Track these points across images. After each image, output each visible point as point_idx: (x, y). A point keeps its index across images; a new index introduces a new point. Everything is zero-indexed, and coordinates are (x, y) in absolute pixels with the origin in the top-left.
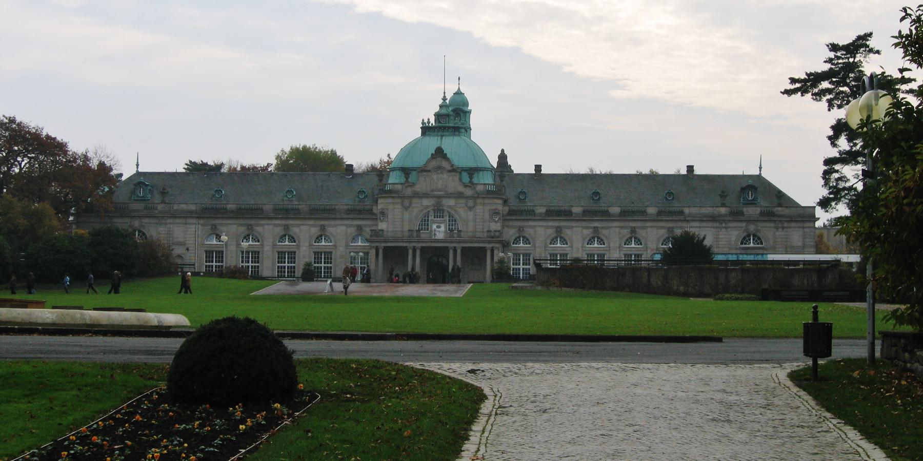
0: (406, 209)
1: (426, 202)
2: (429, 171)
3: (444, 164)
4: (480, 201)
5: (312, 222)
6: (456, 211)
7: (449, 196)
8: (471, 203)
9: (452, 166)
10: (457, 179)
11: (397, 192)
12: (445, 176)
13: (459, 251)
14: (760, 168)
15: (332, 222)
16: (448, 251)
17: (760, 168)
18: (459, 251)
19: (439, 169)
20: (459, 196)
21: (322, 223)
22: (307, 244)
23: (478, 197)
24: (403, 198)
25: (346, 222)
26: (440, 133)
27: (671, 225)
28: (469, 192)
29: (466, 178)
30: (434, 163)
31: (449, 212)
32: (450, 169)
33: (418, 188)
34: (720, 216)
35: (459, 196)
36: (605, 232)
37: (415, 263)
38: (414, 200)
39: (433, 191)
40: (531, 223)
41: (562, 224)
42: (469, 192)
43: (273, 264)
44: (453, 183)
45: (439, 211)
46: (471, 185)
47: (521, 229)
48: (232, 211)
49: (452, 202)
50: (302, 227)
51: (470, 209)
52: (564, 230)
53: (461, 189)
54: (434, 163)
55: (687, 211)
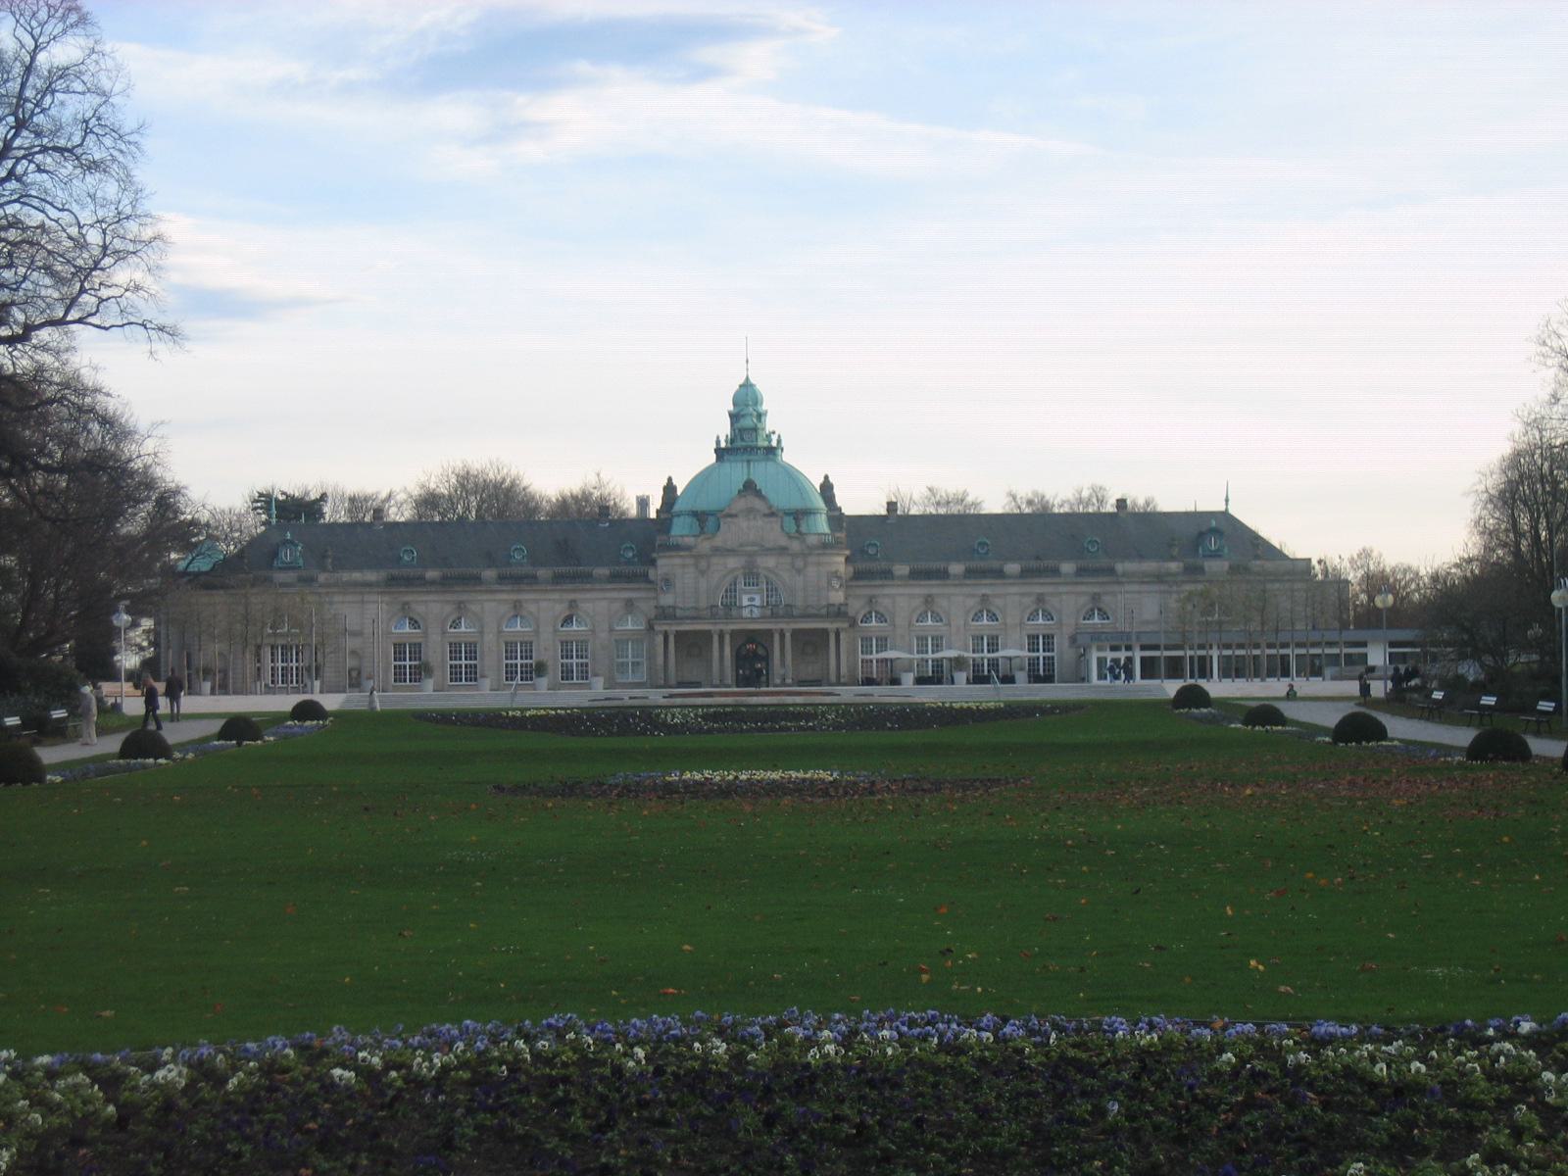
0: (703, 573)
1: (732, 562)
2: (736, 516)
3: (758, 504)
4: (811, 559)
5: (556, 596)
6: (777, 575)
7: (768, 551)
8: (799, 563)
9: (770, 507)
10: (777, 527)
11: (689, 548)
12: (760, 523)
13: (788, 635)
14: (1227, 501)
15: (588, 595)
16: (772, 636)
17: (1227, 501)
18: (788, 635)
19: (750, 511)
20: (782, 551)
21: (572, 596)
22: (551, 629)
23: (810, 554)
24: (698, 557)
25: (609, 595)
26: (745, 457)
27: (1096, 589)
28: (795, 546)
29: (789, 523)
30: (742, 504)
31: (766, 577)
32: (767, 511)
33: (718, 541)
34: (1170, 574)
35: (782, 551)
36: (998, 602)
37: (723, 657)
38: (714, 560)
39: (741, 545)
40: (887, 591)
41: (934, 591)
42: (795, 546)
43: (500, 661)
44: (774, 533)
45: (751, 575)
46: (800, 535)
47: (871, 600)
48: (433, 583)
49: (770, 562)
50: (543, 604)
51: (799, 571)
52: (525, 605)
53: (783, 541)
54: (742, 504)
55: (1119, 567)
